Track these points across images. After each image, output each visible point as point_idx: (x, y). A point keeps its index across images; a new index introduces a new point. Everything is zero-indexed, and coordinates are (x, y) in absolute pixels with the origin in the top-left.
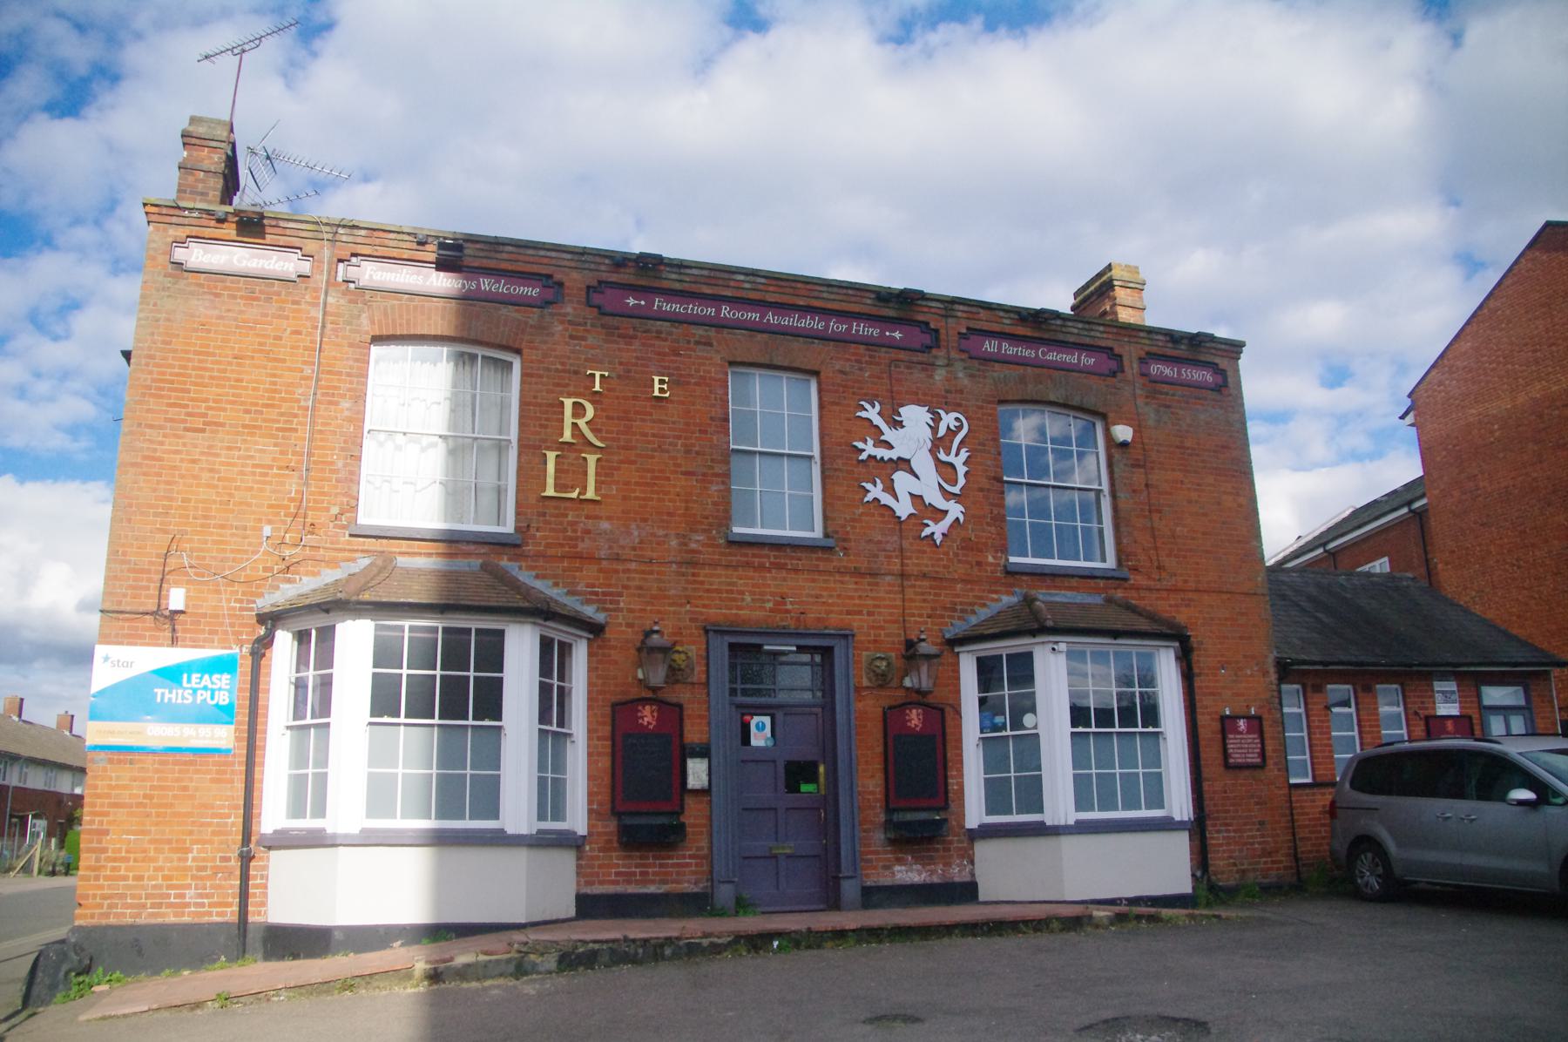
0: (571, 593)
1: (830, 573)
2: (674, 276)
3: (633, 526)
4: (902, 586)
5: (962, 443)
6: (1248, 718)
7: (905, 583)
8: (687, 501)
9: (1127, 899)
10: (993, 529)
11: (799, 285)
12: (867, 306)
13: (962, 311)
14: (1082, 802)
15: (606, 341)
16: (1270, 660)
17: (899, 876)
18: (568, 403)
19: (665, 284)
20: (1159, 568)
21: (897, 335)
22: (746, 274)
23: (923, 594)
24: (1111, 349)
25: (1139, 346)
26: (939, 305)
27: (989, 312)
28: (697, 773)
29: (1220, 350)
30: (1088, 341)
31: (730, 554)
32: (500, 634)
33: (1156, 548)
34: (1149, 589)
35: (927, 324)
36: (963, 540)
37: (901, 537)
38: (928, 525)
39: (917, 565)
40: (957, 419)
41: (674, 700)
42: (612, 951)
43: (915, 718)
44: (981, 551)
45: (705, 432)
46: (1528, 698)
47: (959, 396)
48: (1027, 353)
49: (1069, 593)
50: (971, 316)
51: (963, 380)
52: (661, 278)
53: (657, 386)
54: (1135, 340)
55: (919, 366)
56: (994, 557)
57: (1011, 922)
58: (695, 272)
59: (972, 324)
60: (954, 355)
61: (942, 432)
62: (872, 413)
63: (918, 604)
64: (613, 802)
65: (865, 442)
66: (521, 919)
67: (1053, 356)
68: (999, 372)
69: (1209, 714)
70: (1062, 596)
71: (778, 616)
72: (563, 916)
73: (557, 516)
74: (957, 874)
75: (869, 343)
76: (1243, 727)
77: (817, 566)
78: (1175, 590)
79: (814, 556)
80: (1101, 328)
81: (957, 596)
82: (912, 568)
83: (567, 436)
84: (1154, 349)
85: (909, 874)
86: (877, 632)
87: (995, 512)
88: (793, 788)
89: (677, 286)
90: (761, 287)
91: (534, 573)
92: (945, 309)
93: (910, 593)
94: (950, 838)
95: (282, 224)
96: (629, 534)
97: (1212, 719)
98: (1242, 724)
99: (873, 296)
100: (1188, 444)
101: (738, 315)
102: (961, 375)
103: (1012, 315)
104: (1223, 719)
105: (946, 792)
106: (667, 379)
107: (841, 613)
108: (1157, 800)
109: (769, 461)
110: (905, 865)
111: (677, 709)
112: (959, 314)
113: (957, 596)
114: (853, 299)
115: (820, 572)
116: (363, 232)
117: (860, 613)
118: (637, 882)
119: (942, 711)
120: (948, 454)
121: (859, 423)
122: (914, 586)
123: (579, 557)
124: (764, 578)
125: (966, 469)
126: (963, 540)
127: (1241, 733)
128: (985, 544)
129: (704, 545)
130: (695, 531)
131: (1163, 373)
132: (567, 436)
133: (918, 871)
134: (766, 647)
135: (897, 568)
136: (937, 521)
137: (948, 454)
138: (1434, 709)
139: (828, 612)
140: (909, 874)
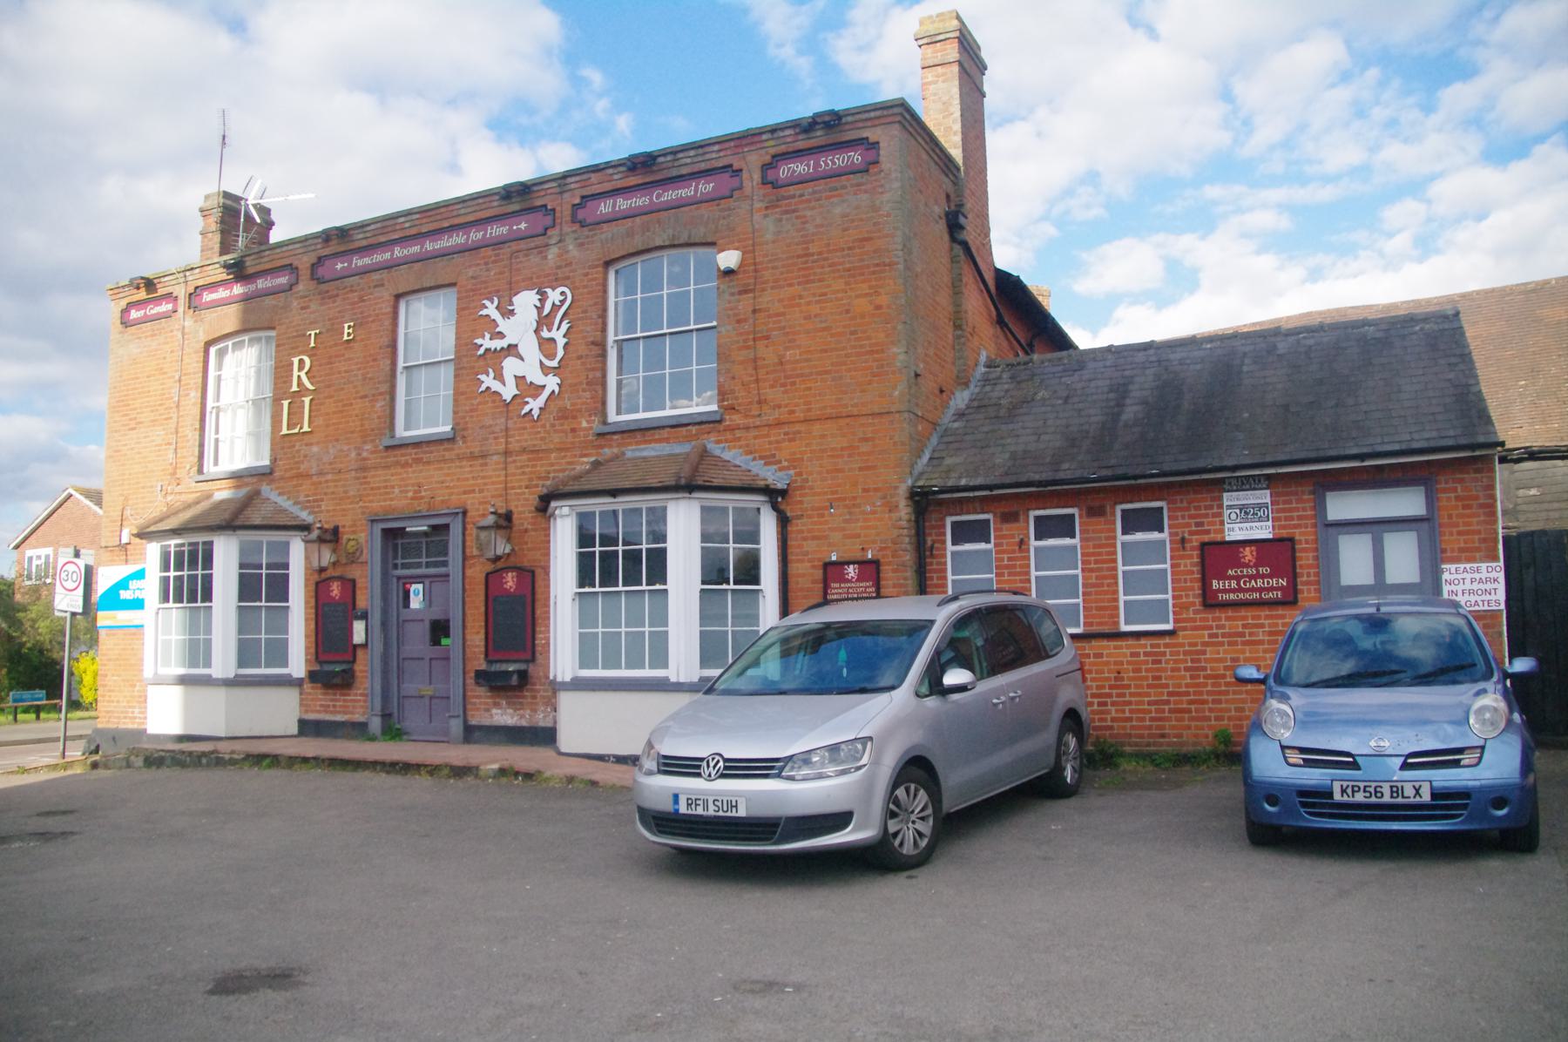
0: (296, 503)
1: (452, 461)
2: (361, 236)
3: (330, 445)
4: (506, 463)
5: (565, 314)
6: (862, 563)
7: (510, 459)
8: (362, 420)
9: (615, 756)
10: (587, 394)
11: (443, 210)
12: (496, 207)
13: (576, 182)
14: (586, 660)
15: (322, 305)
16: (903, 490)
17: (496, 718)
18: (296, 361)
19: (357, 244)
20: (759, 402)
21: (523, 226)
22: (405, 216)
23: (522, 467)
24: (731, 166)
25: (763, 151)
26: (554, 184)
27: (600, 174)
28: (359, 631)
29: (870, 119)
30: (703, 166)
31: (386, 457)
32: (211, 543)
33: (757, 381)
34: (747, 428)
35: (545, 206)
36: (560, 410)
37: (507, 419)
38: (527, 403)
39: (518, 441)
40: (563, 293)
41: (351, 577)
42: (173, 758)
43: (510, 581)
44: (574, 417)
45: (375, 360)
46: (1430, 501)
47: (567, 269)
48: (640, 201)
49: (657, 446)
50: (583, 184)
51: (573, 251)
52: (353, 241)
53: (346, 331)
54: (758, 146)
55: (535, 251)
56: (588, 422)
57: (371, 762)
58: (373, 227)
59: (586, 192)
60: (567, 229)
61: (547, 310)
62: (491, 310)
63: (518, 477)
64: (317, 653)
65: (483, 337)
66: (223, 735)
67: (670, 195)
68: (608, 231)
69: (809, 561)
70: (652, 450)
71: (416, 502)
72: (289, 733)
73: (289, 448)
74: (541, 720)
75: (499, 243)
76: (852, 574)
77: (444, 456)
78: (779, 424)
79: (442, 447)
80: (716, 148)
81: (552, 465)
82: (514, 446)
83: (295, 388)
84: (783, 148)
85: (504, 716)
86: (485, 506)
87: (590, 376)
88: (435, 642)
89: (364, 243)
90: (417, 222)
91: (763, 462)
92: (559, 186)
93: (511, 469)
94: (538, 687)
95: (163, 280)
96: (328, 452)
97: (814, 567)
98: (851, 571)
99: (497, 197)
100: (813, 249)
101: (405, 252)
102: (571, 247)
103: (622, 169)
104: (828, 565)
105: (534, 645)
106: (352, 324)
107: (458, 494)
108: (661, 659)
109: (432, 370)
110: (500, 708)
111: (1289, 543)
112: (573, 186)
113: (552, 465)
114: (484, 206)
115: (445, 461)
116: (197, 270)
117: (473, 491)
118: (331, 712)
119: (533, 572)
120: (549, 330)
121: (482, 321)
122: (514, 461)
123: (299, 476)
124: (407, 473)
125: (565, 340)
126: (560, 410)
127: (1247, 566)
128: (580, 411)
129: (372, 452)
130: (365, 442)
131: (794, 171)
132: (295, 388)
133: (510, 714)
134: (408, 529)
135: (502, 448)
136: (535, 397)
137: (549, 330)
138: (1222, 531)
139: (452, 494)
140: (504, 716)
